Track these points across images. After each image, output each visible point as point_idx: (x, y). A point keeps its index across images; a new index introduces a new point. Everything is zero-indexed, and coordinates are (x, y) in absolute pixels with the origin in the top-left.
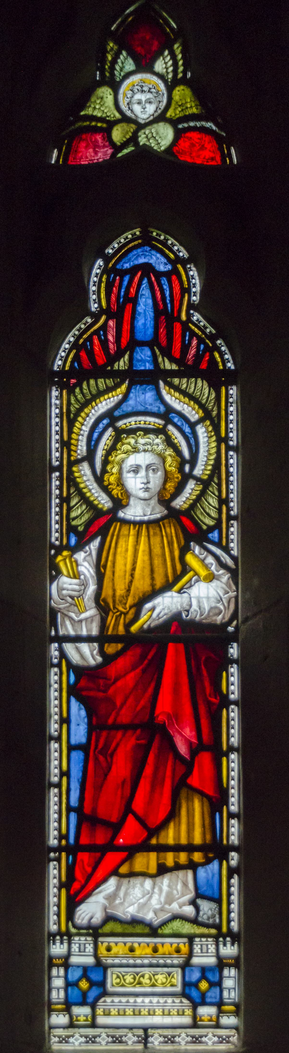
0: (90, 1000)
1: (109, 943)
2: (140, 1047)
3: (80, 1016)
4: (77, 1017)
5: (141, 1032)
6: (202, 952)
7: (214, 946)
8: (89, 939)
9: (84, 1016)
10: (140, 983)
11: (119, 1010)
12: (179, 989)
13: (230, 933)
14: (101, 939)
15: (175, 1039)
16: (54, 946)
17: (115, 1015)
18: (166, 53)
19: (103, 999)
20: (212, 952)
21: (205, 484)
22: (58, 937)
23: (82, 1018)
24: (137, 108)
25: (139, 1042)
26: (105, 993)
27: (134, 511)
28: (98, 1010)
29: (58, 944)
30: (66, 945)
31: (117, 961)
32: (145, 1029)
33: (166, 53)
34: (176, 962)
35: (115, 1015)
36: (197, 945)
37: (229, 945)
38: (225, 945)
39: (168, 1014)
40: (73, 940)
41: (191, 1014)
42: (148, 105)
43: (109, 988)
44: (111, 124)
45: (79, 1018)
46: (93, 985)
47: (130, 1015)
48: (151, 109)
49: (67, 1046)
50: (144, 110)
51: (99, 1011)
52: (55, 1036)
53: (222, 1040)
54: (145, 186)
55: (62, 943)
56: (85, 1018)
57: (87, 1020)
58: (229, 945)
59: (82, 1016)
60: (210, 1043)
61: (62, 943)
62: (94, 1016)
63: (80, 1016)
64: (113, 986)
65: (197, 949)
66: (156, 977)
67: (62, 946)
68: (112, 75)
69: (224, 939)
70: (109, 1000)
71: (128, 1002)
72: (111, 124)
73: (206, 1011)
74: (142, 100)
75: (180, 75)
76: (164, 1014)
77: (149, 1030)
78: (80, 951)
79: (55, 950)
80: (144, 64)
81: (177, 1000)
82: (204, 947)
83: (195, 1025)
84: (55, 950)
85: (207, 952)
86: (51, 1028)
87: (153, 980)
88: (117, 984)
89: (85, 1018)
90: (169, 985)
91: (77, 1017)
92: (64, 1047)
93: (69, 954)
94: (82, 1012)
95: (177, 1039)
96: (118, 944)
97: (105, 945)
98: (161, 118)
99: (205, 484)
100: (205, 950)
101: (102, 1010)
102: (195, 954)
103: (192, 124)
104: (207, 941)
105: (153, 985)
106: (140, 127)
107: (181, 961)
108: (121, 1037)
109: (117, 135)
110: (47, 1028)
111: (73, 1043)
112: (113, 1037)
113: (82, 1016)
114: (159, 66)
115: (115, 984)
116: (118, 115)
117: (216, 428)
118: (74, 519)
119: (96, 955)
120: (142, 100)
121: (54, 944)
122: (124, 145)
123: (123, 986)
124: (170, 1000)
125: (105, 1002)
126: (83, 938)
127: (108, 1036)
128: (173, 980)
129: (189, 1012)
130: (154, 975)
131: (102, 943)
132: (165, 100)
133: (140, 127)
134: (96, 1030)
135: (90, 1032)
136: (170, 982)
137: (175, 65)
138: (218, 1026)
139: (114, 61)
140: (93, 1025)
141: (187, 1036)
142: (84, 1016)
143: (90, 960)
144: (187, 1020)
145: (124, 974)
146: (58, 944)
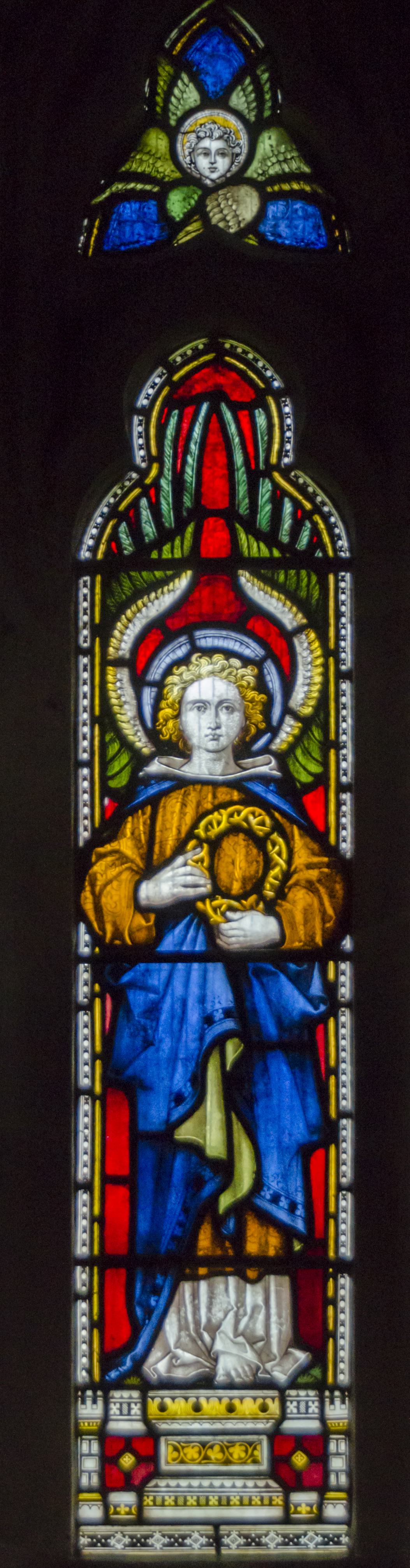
0: (137, 1482)
1: (162, 1398)
2: (212, 1551)
3: (300, 1505)
4: (296, 1507)
5: (209, 1530)
6: (299, 1413)
7: (317, 1404)
8: (312, 1393)
9: (308, 1505)
10: (206, 1458)
11: (198, 1497)
12: (264, 1466)
13: (335, 1387)
14: (151, 1394)
15: (186, 1541)
16: (83, 1406)
17: (214, 1505)
18: (248, 81)
19: (153, 1483)
20: (313, 1413)
21: (307, 723)
22: (89, 1393)
23: (304, 1509)
24: (203, 163)
25: (210, 1545)
26: (157, 1474)
27: (201, 765)
28: (145, 1498)
29: (89, 1402)
30: (100, 1402)
31: (176, 1426)
32: (216, 1524)
33: (248, 81)
34: (260, 1426)
35: (214, 1505)
36: (115, 1403)
37: (337, 1402)
38: (332, 1402)
39: (250, 1505)
40: (113, 1398)
41: (281, 1503)
42: (219, 159)
43: (164, 1467)
44: (167, 187)
45: (118, 1509)
46: (135, 1461)
47: (192, 1505)
48: (223, 164)
49: (147, 1551)
50: (212, 165)
51: (148, 1501)
52: (83, 1536)
53: (328, 1540)
54: (217, 280)
55: (94, 1402)
56: (308, 1509)
57: (311, 1512)
58: (337, 1402)
59: (303, 1505)
60: (234, 1546)
61: (94, 1402)
62: (140, 1507)
63: (300, 1505)
64: (167, 1463)
65: (291, 1407)
66: (231, 1450)
67: (94, 1406)
68: (166, 109)
69: (332, 1392)
70: (162, 1483)
71: (211, 1486)
72: (167, 187)
73: (304, 1500)
74: (216, 152)
75: (267, 113)
76: (176, 1505)
77: (222, 1527)
78: (299, 1413)
79: (84, 1412)
80: (215, 99)
81: (261, 1483)
82: (125, 1411)
83: (287, 1520)
84: (84, 1412)
85: (307, 1413)
86: (79, 1524)
87: (227, 1453)
88: (174, 1460)
89: (308, 1509)
90: (249, 1461)
91: (115, 1507)
92: (99, 1551)
93: (106, 1419)
94: (124, 1500)
95: (264, 1540)
96: (176, 1400)
97: (157, 1401)
98: (236, 179)
99: (307, 723)
100: (125, 1411)
101: (151, 1498)
102: (289, 1416)
103: (286, 187)
104: (307, 1396)
105: (227, 1462)
106: (208, 192)
107: (269, 1425)
108: (260, 1537)
109: (177, 204)
110: (354, 1523)
111: (306, 1545)
112: (170, 1537)
113: (303, 1505)
114: (238, 100)
115: (170, 1460)
116: (177, 175)
117: (323, 638)
118: (112, 777)
119: (145, 1419)
120: (216, 152)
121: (83, 1402)
122: (188, 218)
123: (182, 1462)
124: (250, 1483)
125: (156, 1486)
126: (302, 1393)
127: (277, 1535)
128: (256, 1453)
129: (279, 1499)
130: (228, 1448)
131: (153, 1398)
132: (245, 150)
133: (208, 192)
134: (145, 1528)
135: (140, 1531)
136: (252, 1455)
137: (260, 99)
138: (319, 1519)
139: (169, 93)
140: (140, 1520)
141: (124, 1536)
142: (126, 1506)
143: (138, 1427)
144: (276, 1512)
145: (183, 1444)
146: (89, 1402)
